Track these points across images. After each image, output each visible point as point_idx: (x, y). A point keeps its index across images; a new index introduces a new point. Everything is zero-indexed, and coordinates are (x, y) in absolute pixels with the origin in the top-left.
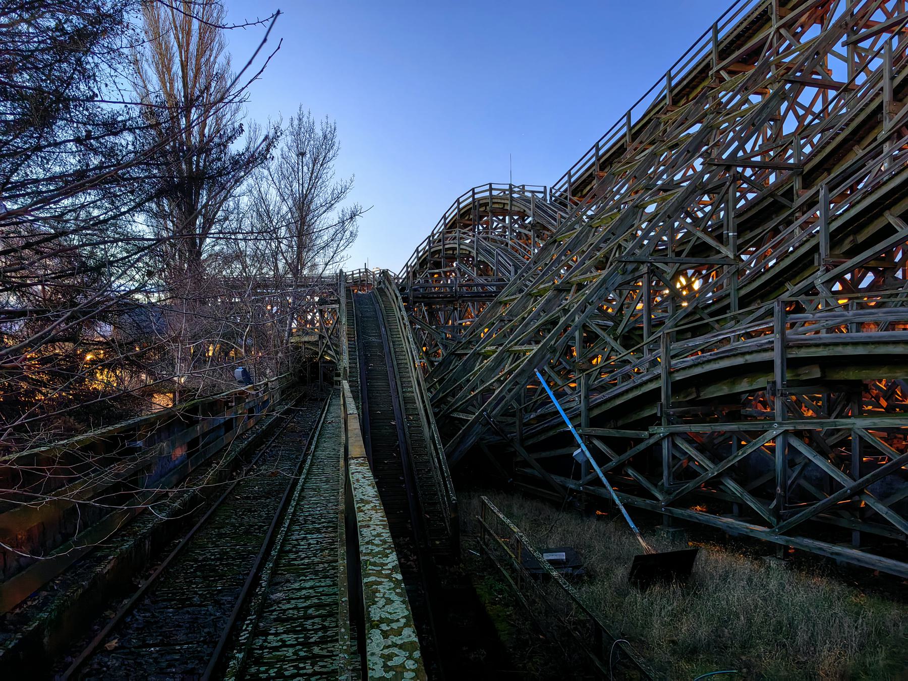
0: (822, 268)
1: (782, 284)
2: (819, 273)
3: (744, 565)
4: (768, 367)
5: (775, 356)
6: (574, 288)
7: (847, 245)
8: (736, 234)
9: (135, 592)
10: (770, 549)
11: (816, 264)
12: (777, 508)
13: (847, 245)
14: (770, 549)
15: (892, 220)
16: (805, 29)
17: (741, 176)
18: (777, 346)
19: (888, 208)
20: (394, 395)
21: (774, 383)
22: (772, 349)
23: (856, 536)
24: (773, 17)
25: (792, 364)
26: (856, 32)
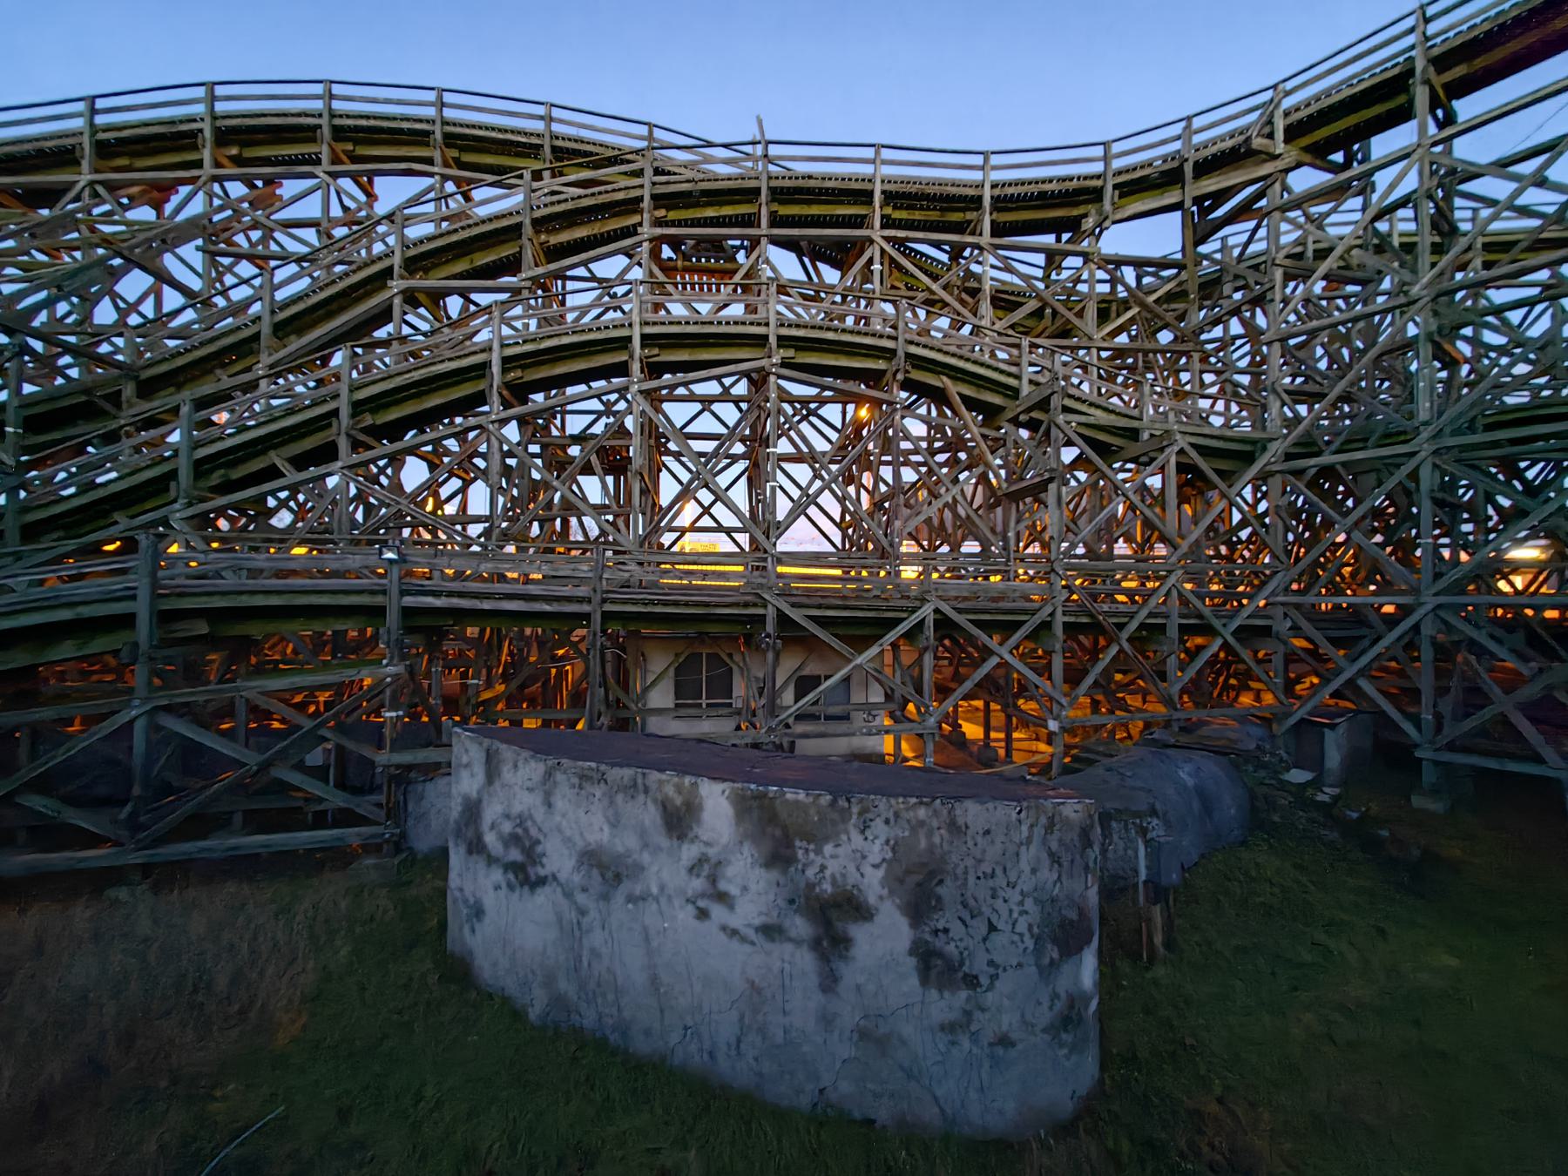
0: (182, 501)
1: (107, 514)
2: (177, 506)
3: (81, 915)
4: (128, 621)
5: (142, 609)
6: (1188, 169)
7: (216, 478)
8: (21, 431)
9: (759, 194)
10: (112, 876)
11: (173, 494)
12: (133, 815)
13: (216, 478)
14: (112, 876)
15: (279, 463)
16: (133, 204)
17: (27, 350)
18: (144, 595)
19: (275, 447)
20: (66, 746)
21: (136, 645)
22: (134, 598)
23: (238, 819)
24: (85, 164)
25: (165, 618)
26: (215, 243)
